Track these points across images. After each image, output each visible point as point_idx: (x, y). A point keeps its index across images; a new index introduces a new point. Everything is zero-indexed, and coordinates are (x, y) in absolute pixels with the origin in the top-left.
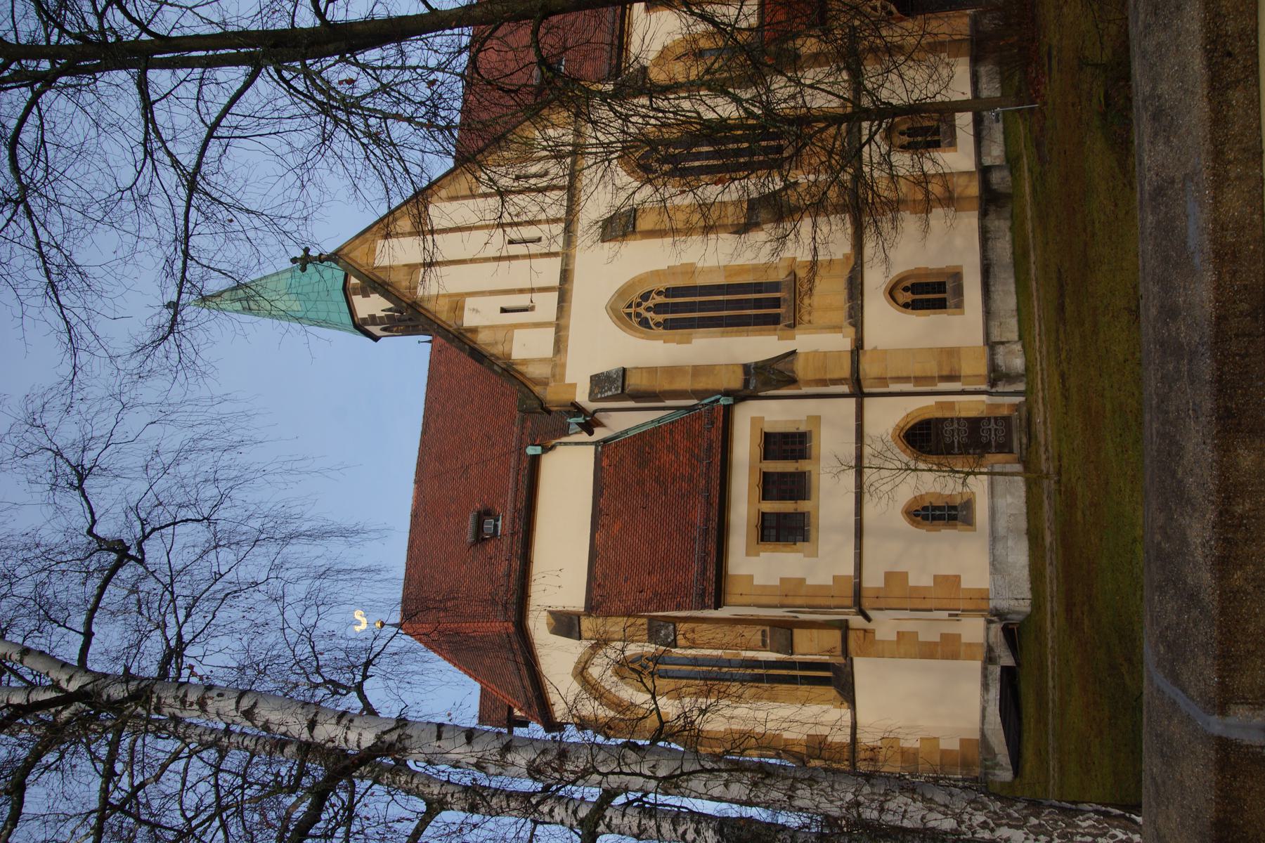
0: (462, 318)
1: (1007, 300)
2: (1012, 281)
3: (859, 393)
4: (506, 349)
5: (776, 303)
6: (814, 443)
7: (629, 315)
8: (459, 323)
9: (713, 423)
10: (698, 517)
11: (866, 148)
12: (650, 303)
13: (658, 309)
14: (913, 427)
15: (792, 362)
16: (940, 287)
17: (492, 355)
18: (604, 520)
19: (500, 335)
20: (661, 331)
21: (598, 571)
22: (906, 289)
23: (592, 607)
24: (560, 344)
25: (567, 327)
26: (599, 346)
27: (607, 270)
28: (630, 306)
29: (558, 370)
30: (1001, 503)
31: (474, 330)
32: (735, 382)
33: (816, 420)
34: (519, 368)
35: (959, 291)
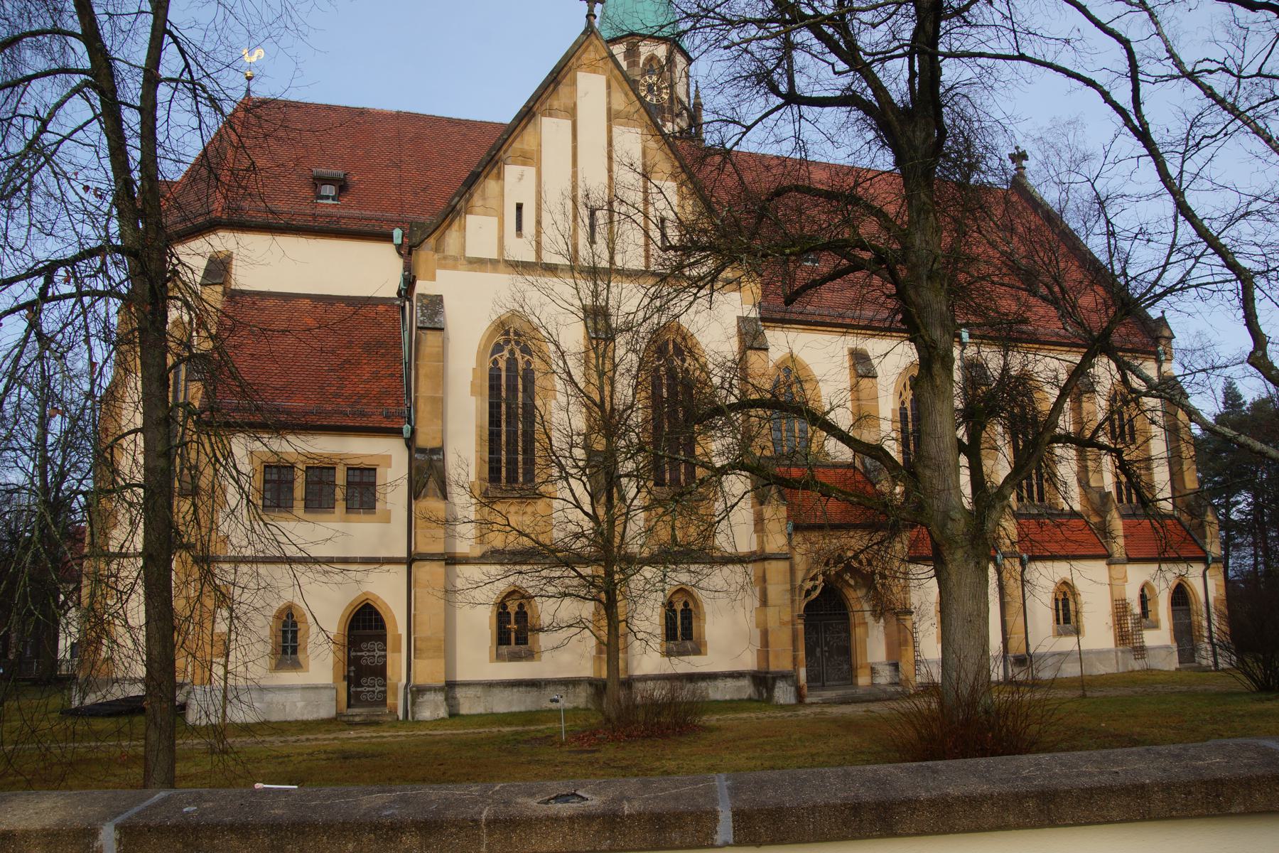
0: (515, 163)
1: (503, 703)
2: (523, 709)
3: (411, 560)
4: (477, 209)
5: (512, 478)
6: (362, 516)
7: (507, 333)
8: (509, 160)
9: (387, 417)
10: (296, 404)
11: (573, 573)
12: (518, 354)
13: (512, 362)
14: (377, 613)
15: (435, 495)
16: (688, 635)
17: (471, 196)
18: (321, 307)
19: (493, 203)
20: (488, 364)
21: (269, 303)
22: (686, 604)
23: (234, 296)
24: (479, 264)
25: (495, 270)
26: (470, 303)
27: (558, 315)
28: (516, 333)
29: (450, 262)
30: (296, 697)
31: (500, 176)
32: (423, 440)
33: (387, 519)
34: (456, 223)
35: (515, 657)
